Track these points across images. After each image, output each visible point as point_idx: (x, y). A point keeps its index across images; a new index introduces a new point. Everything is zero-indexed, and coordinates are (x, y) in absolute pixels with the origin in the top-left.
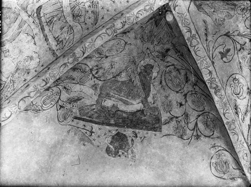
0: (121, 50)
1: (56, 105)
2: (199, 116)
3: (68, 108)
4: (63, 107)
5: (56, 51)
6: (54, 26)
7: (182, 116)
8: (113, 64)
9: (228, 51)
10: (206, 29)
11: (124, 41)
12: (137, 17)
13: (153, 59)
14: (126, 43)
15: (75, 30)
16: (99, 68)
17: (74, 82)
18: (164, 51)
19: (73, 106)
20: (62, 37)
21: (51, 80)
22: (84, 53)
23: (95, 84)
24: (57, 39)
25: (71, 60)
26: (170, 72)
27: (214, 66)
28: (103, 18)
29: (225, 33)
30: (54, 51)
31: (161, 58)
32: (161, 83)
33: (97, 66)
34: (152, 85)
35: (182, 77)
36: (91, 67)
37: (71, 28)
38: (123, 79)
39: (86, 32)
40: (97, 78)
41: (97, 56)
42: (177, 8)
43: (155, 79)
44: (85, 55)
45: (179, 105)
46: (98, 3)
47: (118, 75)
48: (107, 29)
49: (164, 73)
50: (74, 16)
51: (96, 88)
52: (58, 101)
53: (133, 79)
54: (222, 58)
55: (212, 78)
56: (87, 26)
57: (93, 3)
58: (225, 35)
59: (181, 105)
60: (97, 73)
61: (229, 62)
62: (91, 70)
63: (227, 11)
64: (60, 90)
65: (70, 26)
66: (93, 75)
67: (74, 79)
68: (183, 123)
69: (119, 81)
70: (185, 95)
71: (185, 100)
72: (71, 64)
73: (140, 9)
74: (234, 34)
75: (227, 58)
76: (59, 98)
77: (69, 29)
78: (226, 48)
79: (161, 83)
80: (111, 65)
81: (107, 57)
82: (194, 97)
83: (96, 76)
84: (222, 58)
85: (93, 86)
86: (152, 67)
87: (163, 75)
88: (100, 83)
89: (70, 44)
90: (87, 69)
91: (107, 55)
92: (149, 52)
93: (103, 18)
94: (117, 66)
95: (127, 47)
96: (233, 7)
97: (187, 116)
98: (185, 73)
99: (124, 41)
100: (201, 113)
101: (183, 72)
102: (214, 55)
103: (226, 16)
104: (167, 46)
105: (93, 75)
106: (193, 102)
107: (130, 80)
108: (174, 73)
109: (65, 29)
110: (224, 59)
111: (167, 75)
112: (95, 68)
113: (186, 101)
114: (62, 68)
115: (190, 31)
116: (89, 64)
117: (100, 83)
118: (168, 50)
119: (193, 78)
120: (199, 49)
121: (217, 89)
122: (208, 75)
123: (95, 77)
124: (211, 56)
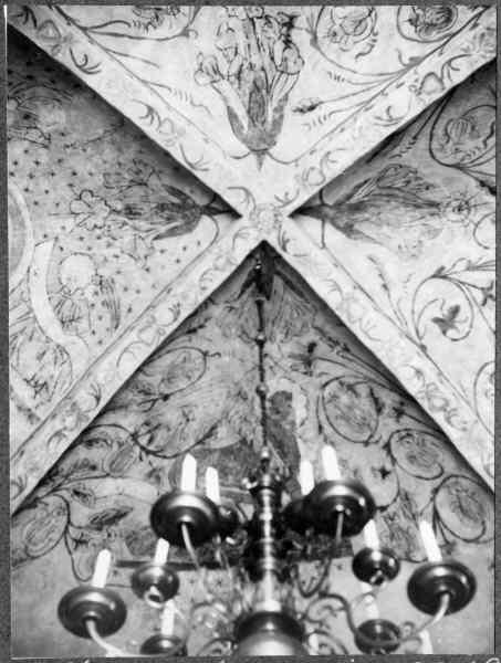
0: (197, 374)
1: (62, 541)
2: (436, 491)
3: (97, 542)
4: (85, 542)
5: (33, 410)
6: (21, 355)
7: (395, 500)
8: (186, 410)
9: (455, 311)
10: (381, 275)
11: (200, 350)
12: (204, 289)
13: (285, 377)
14: (205, 354)
15: (72, 353)
16: (153, 428)
17: (96, 473)
18: (304, 352)
19: (109, 535)
20: (43, 377)
21: (30, 479)
22: (98, 399)
23: (154, 470)
24: (32, 383)
25: (70, 421)
26: (334, 397)
27: (428, 356)
28: (130, 310)
29: (432, 273)
30: (29, 410)
31: (302, 369)
32: (320, 428)
33: (147, 424)
34: (299, 440)
35: (365, 405)
36: (132, 430)
37: (61, 350)
38: (225, 444)
39: (99, 351)
40: (154, 453)
41: (140, 401)
42: (288, 246)
43: (302, 424)
44: (103, 403)
45: (379, 475)
46: (113, 281)
47: (208, 436)
48: (141, 331)
49: (320, 403)
50: (63, 322)
51: (158, 478)
52: (67, 528)
53: (250, 438)
54: (444, 332)
55: (428, 386)
56: (97, 338)
57: (101, 283)
58: (434, 276)
59: (384, 473)
60: (151, 441)
61: (465, 337)
62: (135, 436)
63: (423, 221)
64: (66, 501)
65: (58, 346)
66: (143, 448)
67: (94, 468)
68: (402, 522)
69: (215, 450)
70: (387, 447)
71: (389, 459)
72: (72, 430)
73: (204, 269)
74: (456, 269)
75: (456, 328)
76: (69, 522)
77: (59, 354)
78: (446, 307)
79: (320, 428)
80: (184, 415)
81: (166, 398)
82: (407, 445)
83: (151, 448)
84: (444, 332)
85: (150, 475)
86: (289, 397)
87: (321, 408)
88: (166, 462)
89: (65, 388)
90: (124, 436)
91: (167, 392)
92: (272, 364)
93: (130, 310)
94: (198, 413)
95: (212, 362)
96: (434, 210)
97: (407, 499)
98: (368, 390)
99: (200, 350)
100: (439, 481)
101: (363, 390)
102: (421, 331)
103: (423, 234)
104: (312, 336)
105: (143, 448)
106: (412, 458)
107: (243, 441)
108: (345, 399)
109: (49, 356)
110: (451, 333)
111: (330, 407)
112: (143, 430)
113: (394, 461)
114: (51, 445)
115: (337, 287)
116: (124, 423)
117: (167, 464)
118: (312, 347)
119: (389, 399)
120: (372, 324)
121: (448, 409)
122: (416, 379)
123: (148, 452)
124: (414, 334)
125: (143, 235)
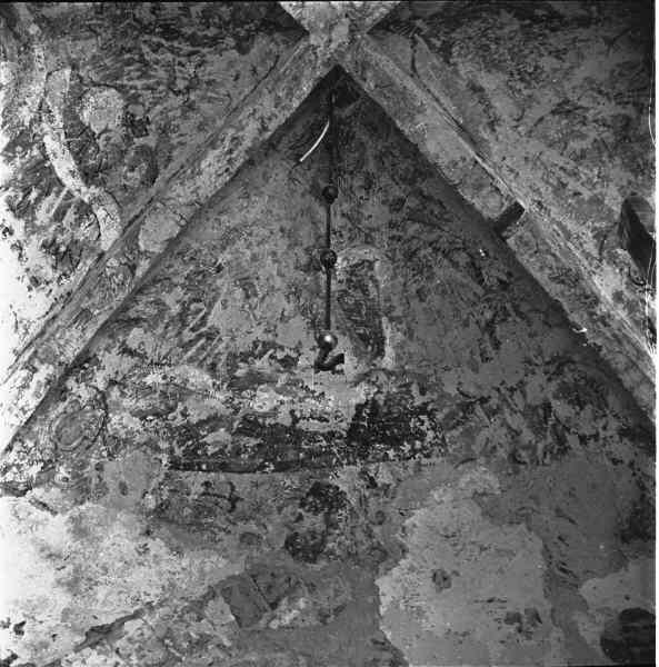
50: (86, 174)
109: (70, 216)
125: (183, 60)
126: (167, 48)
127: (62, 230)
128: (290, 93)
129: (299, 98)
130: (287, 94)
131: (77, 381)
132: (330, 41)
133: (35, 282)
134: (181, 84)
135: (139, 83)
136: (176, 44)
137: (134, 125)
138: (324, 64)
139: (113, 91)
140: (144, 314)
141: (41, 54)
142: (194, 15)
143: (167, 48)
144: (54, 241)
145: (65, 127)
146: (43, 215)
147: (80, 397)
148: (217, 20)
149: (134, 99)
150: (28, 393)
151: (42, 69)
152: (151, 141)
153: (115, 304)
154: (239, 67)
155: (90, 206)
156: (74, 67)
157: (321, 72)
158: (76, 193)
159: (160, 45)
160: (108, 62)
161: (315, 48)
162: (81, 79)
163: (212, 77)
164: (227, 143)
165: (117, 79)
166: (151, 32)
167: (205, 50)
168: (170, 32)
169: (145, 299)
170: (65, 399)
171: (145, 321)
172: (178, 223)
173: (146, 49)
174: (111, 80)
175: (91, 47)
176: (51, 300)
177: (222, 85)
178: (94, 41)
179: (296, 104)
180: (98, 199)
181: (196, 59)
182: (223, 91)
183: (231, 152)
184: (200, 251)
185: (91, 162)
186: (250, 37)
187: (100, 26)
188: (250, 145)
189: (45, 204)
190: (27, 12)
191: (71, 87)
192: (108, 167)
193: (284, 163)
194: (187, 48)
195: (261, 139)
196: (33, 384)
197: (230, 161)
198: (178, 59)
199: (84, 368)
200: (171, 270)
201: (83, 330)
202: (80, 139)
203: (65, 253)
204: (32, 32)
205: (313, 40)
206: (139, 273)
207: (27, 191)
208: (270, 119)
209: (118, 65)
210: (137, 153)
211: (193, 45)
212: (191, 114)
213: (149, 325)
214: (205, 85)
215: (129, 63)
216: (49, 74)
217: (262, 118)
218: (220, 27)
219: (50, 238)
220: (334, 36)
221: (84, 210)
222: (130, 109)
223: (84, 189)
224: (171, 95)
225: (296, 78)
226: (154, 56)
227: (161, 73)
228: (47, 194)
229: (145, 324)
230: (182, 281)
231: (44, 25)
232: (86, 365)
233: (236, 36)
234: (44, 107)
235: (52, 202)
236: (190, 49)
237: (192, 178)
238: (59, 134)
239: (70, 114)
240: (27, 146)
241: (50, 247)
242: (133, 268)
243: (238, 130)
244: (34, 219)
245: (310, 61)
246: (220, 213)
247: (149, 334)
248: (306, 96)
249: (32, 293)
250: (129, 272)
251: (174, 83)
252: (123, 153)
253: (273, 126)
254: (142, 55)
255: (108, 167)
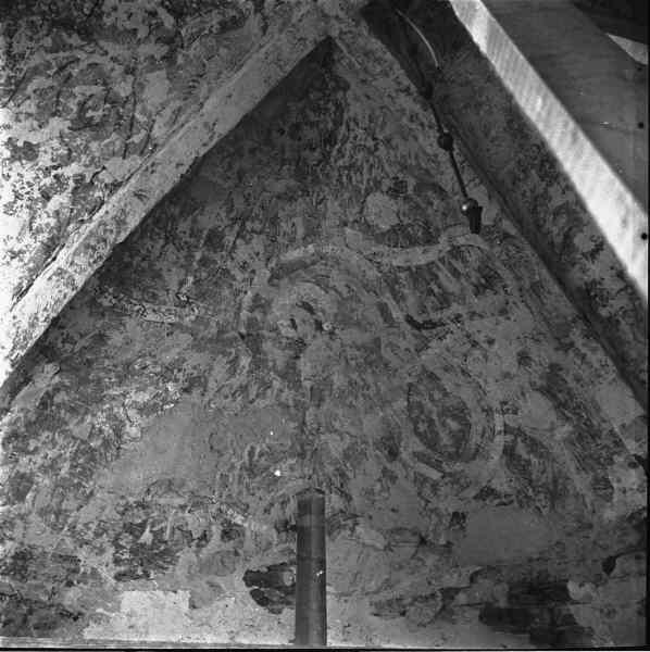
109: (458, 265)
125: (352, 135)
126: (342, 145)
127: (468, 276)
128: (378, 60)
129: (385, 53)
130: (379, 64)
131: (604, 306)
132: (337, 17)
133: (503, 312)
134: (370, 143)
135: (366, 177)
136: (340, 137)
137: (397, 190)
138: (356, 26)
139: (369, 198)
140: (563, 228)
141: (331, 247)
142: (317, 119)
143: (342, 145)
144: (475, 286)
145: (389, 246)
146: (452, 286)
147: (622, 308)
148: (322, 102)
149: (378, 184)
150: (590, 355)
151: (342, 251)
152: (411, 182)
153: (534, 259)
154: (359, 92)
155: (454, 247)
156: (345, 224)
157: (364, 28)
158: (441, 255)
159: (339, 151)
160: (346, 195)
161: (341, 32)
162: (356, 221)
163: (367, 117)
164: (413, 126)
165: (360, 192)
166: (329, 153)
167: (346, 116)
168: (330, 139)
169: (548, 225)
170: (618, 321)
171: (570, 229)
172: (475, 185)
173: (340, 163)
174: (361, 198)
175: (333, 206)
176: (521, 305)
177: (373, 110)
178: (329, 204)
179: (389, 56)
180: (451, 239)
181: (352, 125)
182: (378, 113)
183: (422, 125)
184: (519, 162)
185: (420, 234)
186: (337, 79)
187: (318, 195)
188: (418, 106)
189: (445, 283)
190: (298, 250)
191: (360, 230)
192: (426, 223)
193: (457, 61)
194: (343, 129)
195: (415, 95)
196: (584, 350)
197: (430, 127)
198: (351, 139)
199: (596, 296)
200: (528, 194)
201: (549, 292)
202: (399, 236)
203: (487, 281)
204: (310, 246)
205: (335, 33)
206: (513, 232)
207: (431, 292)
208: (399, 83)
209: (350, 187)
210: (419, 196)
211: (341, 124)
212: (394, 143)
213: (576, 226)
214: (372, 125)
215: (350, 179)
216: (347, 246)
217: (397, 91)
218: (329, 101)
219: (471, 288)
220: (333, 13)
221: (456, 252)
222: (385, 188)
223: (440, 247)
224: (377, 153)
225: (366, 54)
226: (346, 159)
227: (360, 156)
228: (437, 277)
229: (574, 229)
230: (544, 184)
231: (310, 240)
232: (592, 294)
233: (335, 90)
234: (371, 257)
235: (444, 275)
236: (344, 127)
237: (439, 163)
238: (394, 252)
239: (380, 238)
240: (396, 281)
241: (479, 290)
242: (506, 236)
243: (404, 114)
244: (452, 294)
245: (353, 38)
246: (486, 135)
247: (585, 229)
248: (383, 46)
249: (513, 319)
250: (509, 239)
251: (369, 149)
252: (418, 207)
253: (406, 82)
254: (345, 168)
255: (426, 223)
